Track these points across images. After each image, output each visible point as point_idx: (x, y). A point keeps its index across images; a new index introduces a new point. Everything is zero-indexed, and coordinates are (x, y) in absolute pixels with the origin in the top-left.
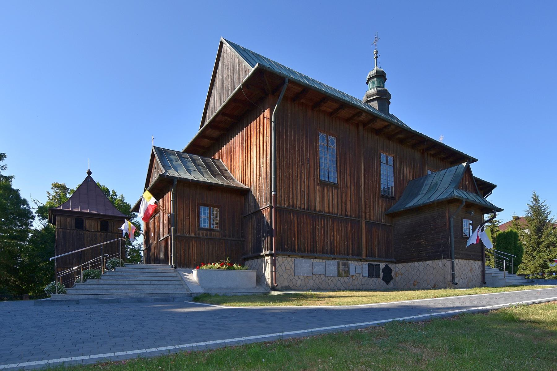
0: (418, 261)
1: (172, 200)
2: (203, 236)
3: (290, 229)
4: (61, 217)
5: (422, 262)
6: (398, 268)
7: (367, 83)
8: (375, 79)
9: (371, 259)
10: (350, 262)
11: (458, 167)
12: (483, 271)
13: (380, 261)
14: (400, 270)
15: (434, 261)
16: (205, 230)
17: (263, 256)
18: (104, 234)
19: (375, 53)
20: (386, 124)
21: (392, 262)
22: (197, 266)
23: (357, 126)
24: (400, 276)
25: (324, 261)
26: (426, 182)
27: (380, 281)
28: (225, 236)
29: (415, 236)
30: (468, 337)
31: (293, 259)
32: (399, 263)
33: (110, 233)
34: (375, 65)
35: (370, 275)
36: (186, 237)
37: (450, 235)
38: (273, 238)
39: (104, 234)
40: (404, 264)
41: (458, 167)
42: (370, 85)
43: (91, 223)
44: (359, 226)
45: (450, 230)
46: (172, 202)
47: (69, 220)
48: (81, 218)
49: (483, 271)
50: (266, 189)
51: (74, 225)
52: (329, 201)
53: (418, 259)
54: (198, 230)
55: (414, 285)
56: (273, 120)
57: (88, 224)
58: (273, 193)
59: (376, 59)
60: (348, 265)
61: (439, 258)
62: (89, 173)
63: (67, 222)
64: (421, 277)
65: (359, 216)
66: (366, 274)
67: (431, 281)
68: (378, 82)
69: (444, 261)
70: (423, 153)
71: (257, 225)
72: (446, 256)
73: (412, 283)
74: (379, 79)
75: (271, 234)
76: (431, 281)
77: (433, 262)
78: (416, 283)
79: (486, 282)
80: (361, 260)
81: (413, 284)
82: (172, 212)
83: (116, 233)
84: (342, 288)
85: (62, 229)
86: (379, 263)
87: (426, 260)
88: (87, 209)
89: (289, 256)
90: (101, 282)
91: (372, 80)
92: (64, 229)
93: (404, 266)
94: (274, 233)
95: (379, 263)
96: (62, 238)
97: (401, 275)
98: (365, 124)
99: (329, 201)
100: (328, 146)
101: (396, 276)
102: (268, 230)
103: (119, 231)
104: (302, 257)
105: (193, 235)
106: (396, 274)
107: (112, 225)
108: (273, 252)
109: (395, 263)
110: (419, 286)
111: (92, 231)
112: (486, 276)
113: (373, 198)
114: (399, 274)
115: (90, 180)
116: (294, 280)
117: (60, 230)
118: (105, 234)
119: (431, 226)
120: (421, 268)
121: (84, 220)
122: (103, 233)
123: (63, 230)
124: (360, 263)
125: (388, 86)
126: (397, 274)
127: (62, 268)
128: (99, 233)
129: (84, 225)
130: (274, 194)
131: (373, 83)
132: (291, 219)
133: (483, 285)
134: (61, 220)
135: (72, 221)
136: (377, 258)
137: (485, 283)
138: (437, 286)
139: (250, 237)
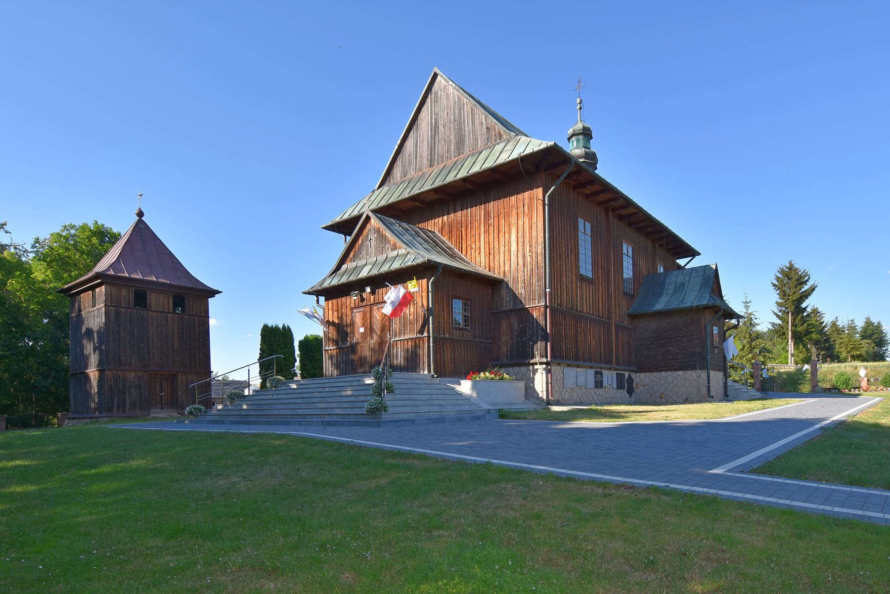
0: (666, 371)
1: (430, 290)
2: (456, 336)
3: (560, 333)
4: (112, 288)
6: (640, 378)
7: (569, 139)
8: (581, 137)
9: (619, 367)
10: (603, 371)
12: (725, 383)
13: (624, 370)
15: (686, 371)
16: (459, 330)
17: (534, 364)
19: (578, 102)
20: (635, 211)
21: (633, 371)
22: (465, 376)
23: (607, 210)
25: (584, 369)
26: (668, 280)
27: (623, 393)
28: (475, 337)
29: (662, 342)
31: (562, 368)
32: (641, 372)
33: (188, 315)
34: (579, 118)
35: (618, 388)
36: (443, 338)
37: (706, 344)
38: (549, 344)
40: (648, 374)
42: (572, 142)
43: (158, 298)
44: (609, 328)
45: (706, 339)
46: (430, 294)
47: (124, 292)
48: (143, 289)
49: (725, 383)
50: (537, 286)
51: (132, 300)
52: (586, 302)
53: (666, 368)
54: (452, 329)
55: (661, 398)
56: (546, 203)
57: (153, 299)
58: (548, 290)
59: (580, 110)
60: (601, 373)
61: (693, 368)
62: (140, 214)
63: (121, 296)
65: (609, 318)
66: (615, 386)
68: (585, 141)
69: (699, 372)
70: (654, 242)
71: (518, 326)
72: (702, 367)
73: (659, 395)
74: (586, 137)
75: (545, 338)
77: (685, 373)
78: (663, 396)
79: (728, 394)
80: (610, 369)
81: (660, 396)
82: (430, 306)
83: (196, 316)
84: (598, 402)
85: (113, 306)
86: (624, 373)
87: (676, 370)
88: (151, 275)
89: (559, 364)
90: (397, 397)
91: (577, 137)
92: (117, 307)
93: (648, 375)
94: (550, 338)
95: (624, 373)
96: (113, 321)
98: (614, 209)
99: (586, 302)
100: (585, 234)
101: (637, 387)
102: (540, 333)
103: (200, 313)
104: (569, 366)
105: (447, 336)
106: (637, 385)
107: (191, 302)
108: (549, 359)
109: (636, 372)
111: (160, 312)
112: (729, 389)
113: (618, 295)
115: (142, 226)
116: (563, 393)
117: (111, 308)
119: (682, 332)
120: (670, 379)
121: (148, 293)
122: (177, 315)
123: (116, 308)
124: (611, 372)
125: (594, 147)
127: (114, 371)
128: (171, 315)
129: (148, 301)
130: (549, 292)
131: (578, 140)
133: (726, 398)
134: (112, 292)
135: (129, 294)
136: (622, 367)
137: (727, 396)
138: (689, 399)
139: (503, 339)
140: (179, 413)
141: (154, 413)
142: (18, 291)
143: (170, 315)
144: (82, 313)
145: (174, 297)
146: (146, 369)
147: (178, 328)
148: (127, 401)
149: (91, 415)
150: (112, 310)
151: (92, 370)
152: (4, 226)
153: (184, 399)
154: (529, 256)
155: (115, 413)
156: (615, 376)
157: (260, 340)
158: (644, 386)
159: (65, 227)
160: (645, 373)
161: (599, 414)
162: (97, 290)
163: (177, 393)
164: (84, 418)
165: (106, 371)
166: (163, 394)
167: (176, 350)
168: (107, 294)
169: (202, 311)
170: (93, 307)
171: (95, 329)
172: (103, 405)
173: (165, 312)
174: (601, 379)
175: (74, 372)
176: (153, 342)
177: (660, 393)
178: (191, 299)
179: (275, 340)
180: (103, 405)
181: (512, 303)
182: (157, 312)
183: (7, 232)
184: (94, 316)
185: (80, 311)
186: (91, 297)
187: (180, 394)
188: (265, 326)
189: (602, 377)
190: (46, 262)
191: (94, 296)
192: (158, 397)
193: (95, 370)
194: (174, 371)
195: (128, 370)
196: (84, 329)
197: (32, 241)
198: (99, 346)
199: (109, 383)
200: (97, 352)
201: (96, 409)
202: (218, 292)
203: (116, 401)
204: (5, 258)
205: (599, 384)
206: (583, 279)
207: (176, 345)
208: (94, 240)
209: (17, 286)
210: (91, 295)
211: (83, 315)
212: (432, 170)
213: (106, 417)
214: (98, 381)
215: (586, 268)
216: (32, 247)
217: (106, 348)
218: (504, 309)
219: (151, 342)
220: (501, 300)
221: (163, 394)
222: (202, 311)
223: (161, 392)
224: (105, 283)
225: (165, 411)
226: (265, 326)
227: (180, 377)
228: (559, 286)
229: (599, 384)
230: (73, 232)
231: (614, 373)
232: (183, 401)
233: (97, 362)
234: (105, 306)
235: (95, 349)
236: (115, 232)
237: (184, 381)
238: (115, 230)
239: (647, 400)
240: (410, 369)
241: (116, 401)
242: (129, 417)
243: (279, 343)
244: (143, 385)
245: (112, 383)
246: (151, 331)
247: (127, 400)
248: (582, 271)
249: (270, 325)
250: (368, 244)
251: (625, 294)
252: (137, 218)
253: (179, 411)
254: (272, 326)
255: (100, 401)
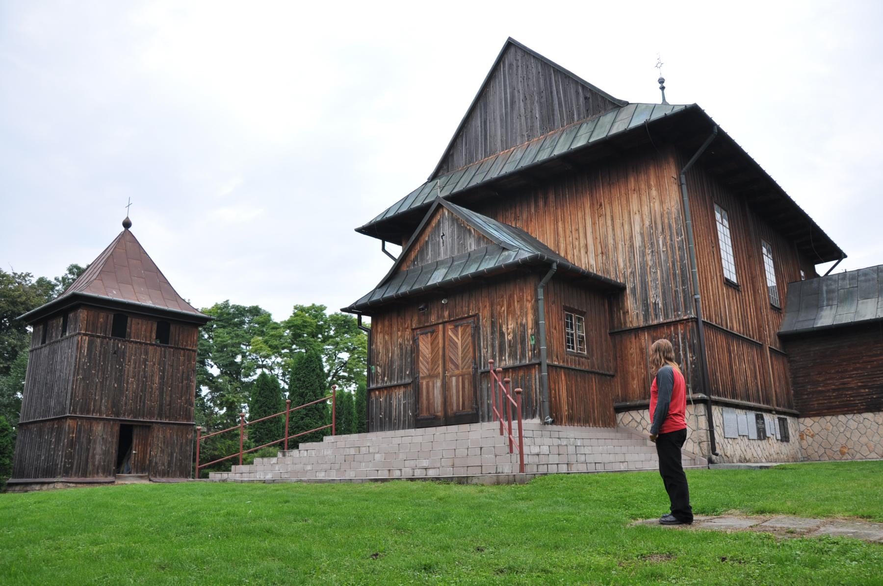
5: (852, 415)
11: (589, 140)
14: (809, 428)
24: (810, 439)
30: (820, 577)
40: (817, 419)
41: (589, 140)
62: (127, 224)
64: (855, 439)
66: (779, 437)
67: (875, 446)
76: (875, 446)
78: (846, 450)
81: (840, 451)
86: (785, 417)
97: (812, 438)
110: (853, 455)
114: (807, 435)
126: (803, 435)
132: (364, 330)
154: (663, 251)
156: (777, 421)
158: (813, 436)
160: (813, 418)
161: (272, 455)
167: (655, 304)
172: (59, 466)
174: (759, 425)
175: (24, 422)
177: (840, 446)
180: (59, 466)
181: (641, 318)
189: (764, 423)
199: (71, 435)
205: (762, 435)
206: (728, 282)
212: (509, 153)
215: (730, 272)
218: (629, 325)
220: (624, 313)
228: (705, 292)
229: (762, 435)
231: (776, 416)
239: (819, 457)
240: (486, 416)
245: (74, 435)
248: (727, 274)
250: (439, 241)
251: (773, 307)
252: (123, 229)
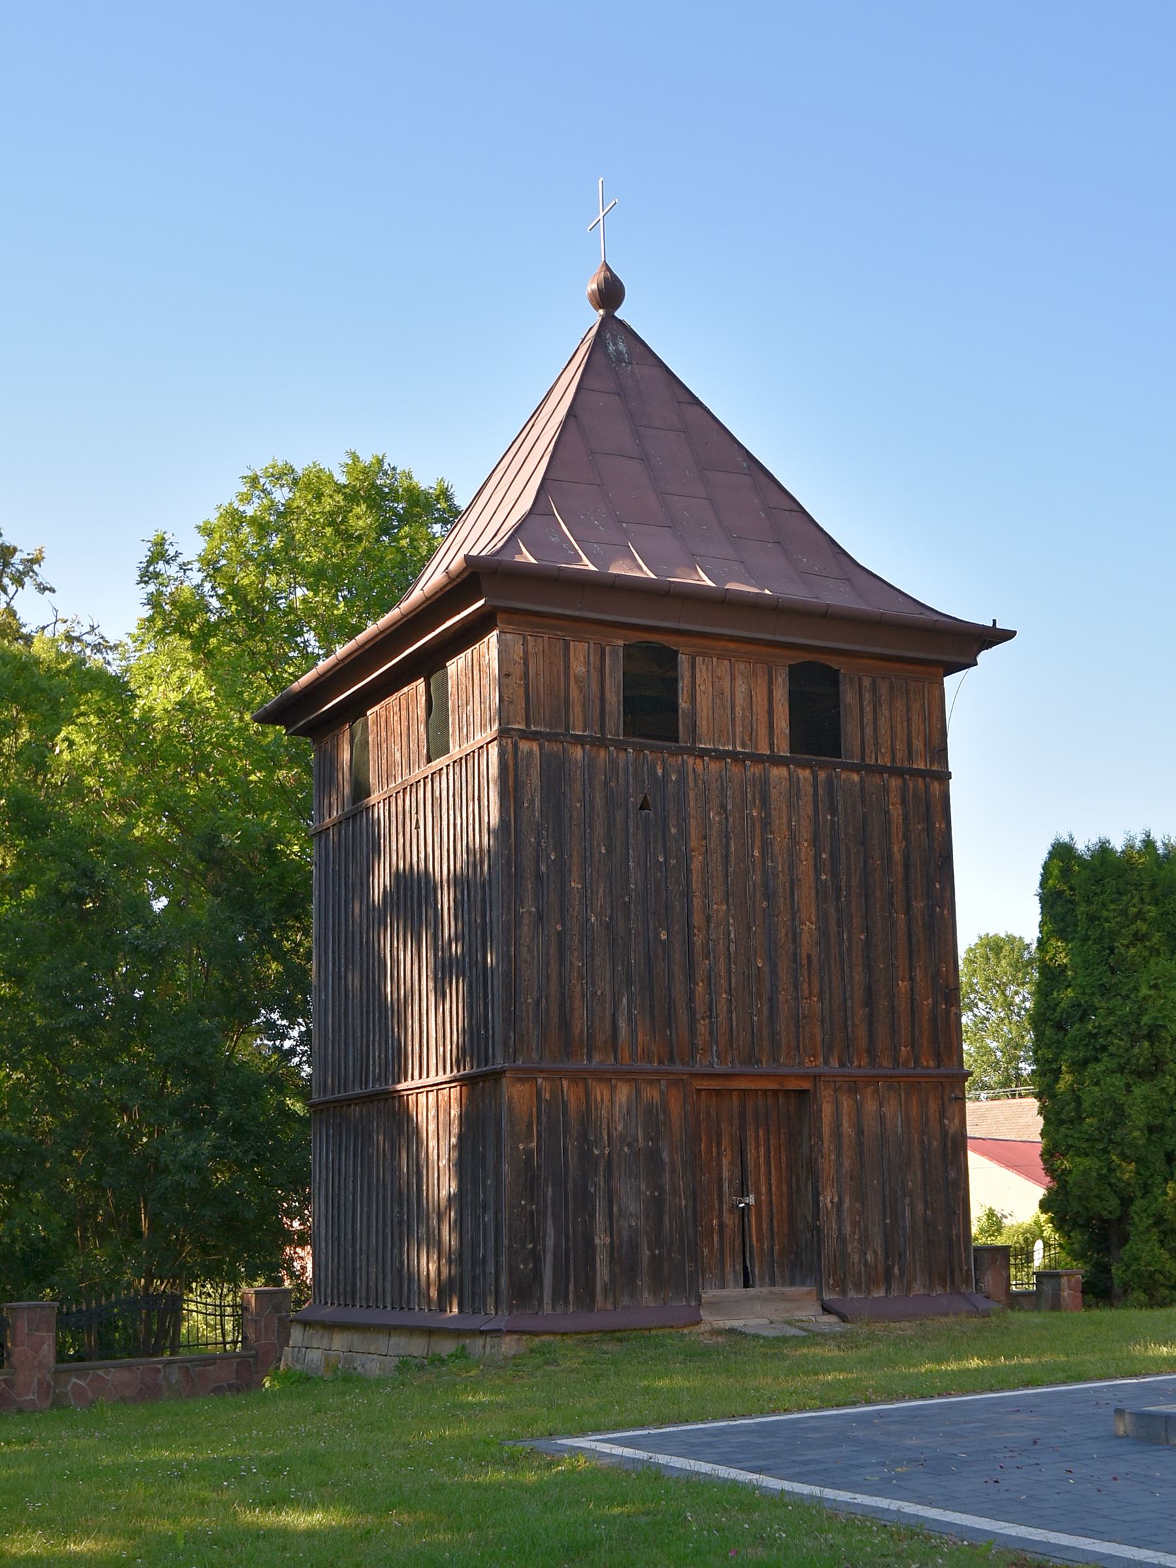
18: (815, 777)
39: (815, 777)
47: (580, 658)
92: (551, 737)
111: (733, 755)
115: (622, 347)
117: (524, 746)
118: (822, 775)
122: (807, 772)
128: (784, 771)
129: (683, 704)
140: (827, 1309)
141: (714, 1305)
142: (88, 772)
143: (778, 773)
144: (374, 798)
145: (796, 673)
146: (678, 1067)
147: (815, 842)
148: (597, 1241)
149: (421, 1316)
150: (531, 752)
151: (425, 1081)
152: (36, 567)
153: (847, 1229)
155: (547, 1308)
157: (1039, 910)
159: (254, 481)
162: (456, 666)
163: (816, 1195)
164: (390, 1330)
165: (505, 1082)
166: (751, 1199)
168: (508, 675)
169: (918, 744)
170: (429, 760)
171: (442, 870)
172: (491, 1269)
173: (758, 759)
176: (708, 919)
178: (867, 682)
179: (1123, 913)
182: (720, 756)
183: (43, 589)
184: (436, 802)
185: (361, 790)
186: (422, 713)
187: (828, 1198)
188: (1062, 853)
190: (190, 636)
191: (436, 708)
192: (728, 1219)
193: (441, 1078)
194: (799, 1077)
195: (603, 1076)
196: (381, 880)
197: (142, 553)
198: (470, 951)
200: (457, 989)
201: (447, 1289)
202: (994, 636)
203: (550, 1242)
204: (37, 662)
207: (809, 928)
208: (361, 519)
209: (86, 750)
210: (423, 700)
211: (380, 812)
213: (510, 1332)
214: (460, 1137)
216: (142, 576)
217: (505, 957)
219: (697, 919)
221: (751, 1199)
222: (918, 744)
223: (743, 1193)
224: (500, 617)
225: (758, 1298)
226: (1062, 853)
227: (827, 1109)
230: (281, 495)
232: (841, 1238)
233: (453, 1038)
234: (503, 733)
235: (443, 973)
236: (423, 486)
237: (847, 1129)
238: (425, 481)
241: (550, 1242)
242: (610, 1333)
243: (1142, 927)
244: (665, 1156)
246: (697, 864)
247: (601, 1240)
249: (1083, 844)
253: (827, 1297)
254: (1104, 849)
255: (474, 1247)
